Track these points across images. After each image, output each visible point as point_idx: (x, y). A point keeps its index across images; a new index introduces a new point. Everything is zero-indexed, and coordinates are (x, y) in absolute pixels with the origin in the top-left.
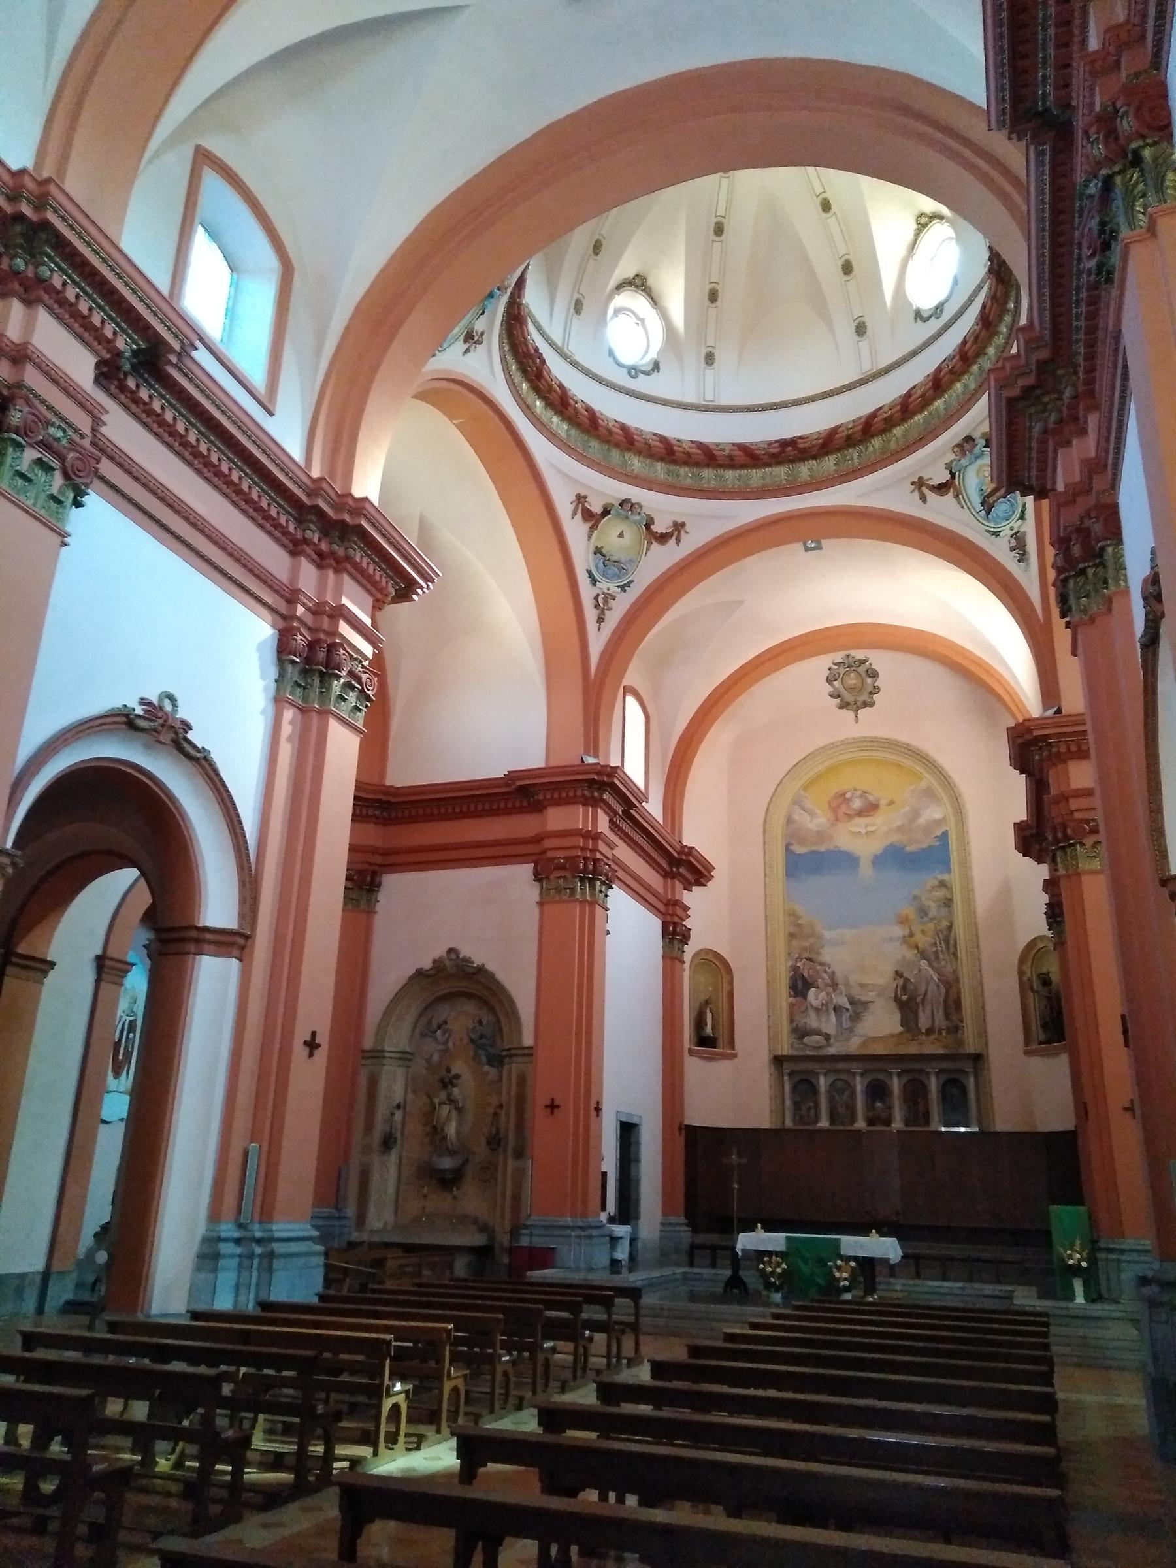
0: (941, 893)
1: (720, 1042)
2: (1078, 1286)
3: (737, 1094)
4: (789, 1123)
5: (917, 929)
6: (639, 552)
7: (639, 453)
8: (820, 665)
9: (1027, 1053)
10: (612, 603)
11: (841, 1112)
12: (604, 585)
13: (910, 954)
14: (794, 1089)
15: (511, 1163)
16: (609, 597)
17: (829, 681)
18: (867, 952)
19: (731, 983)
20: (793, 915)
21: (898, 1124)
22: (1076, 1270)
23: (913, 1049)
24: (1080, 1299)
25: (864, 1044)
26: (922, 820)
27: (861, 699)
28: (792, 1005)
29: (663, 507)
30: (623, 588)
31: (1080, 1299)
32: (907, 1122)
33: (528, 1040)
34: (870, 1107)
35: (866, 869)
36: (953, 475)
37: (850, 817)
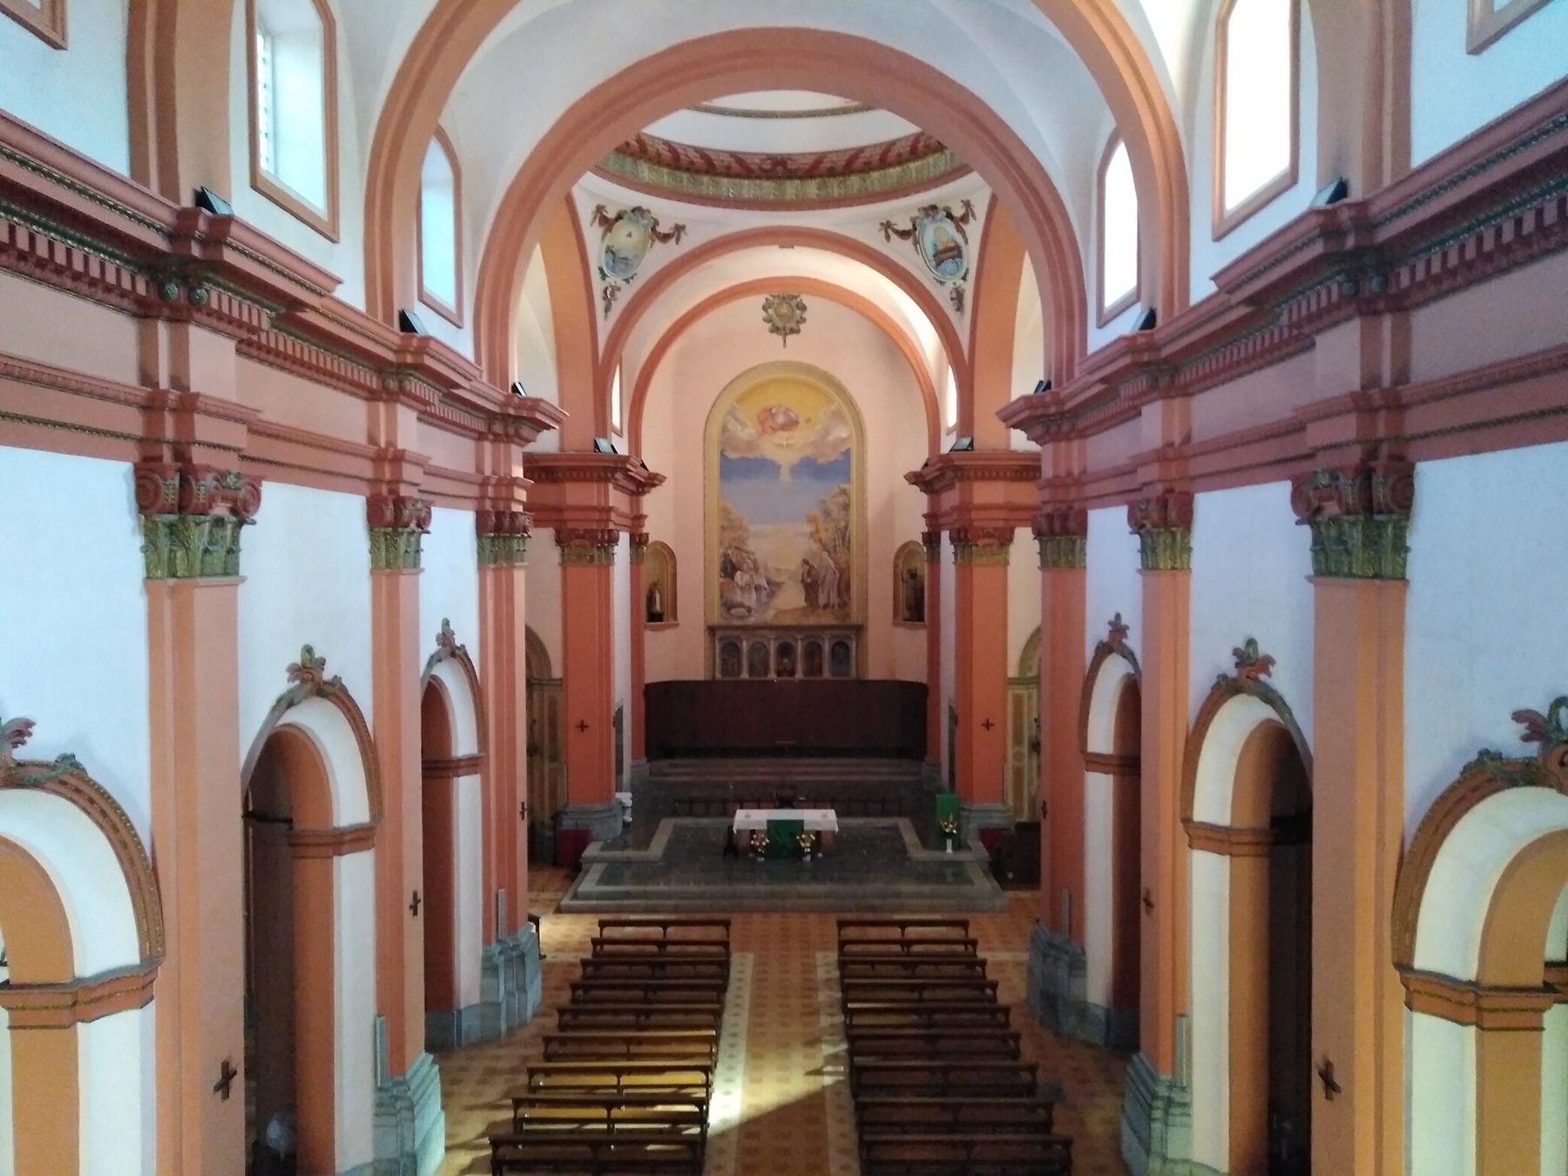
0: (841, 499)
2: (949, 843)
4: (718, 676)
5: (821, 526)
6: (644, 247)
8: (759, 300)
9: (895, 624)
10: (618, 294)
11: (759, 666)
12: (612, 279)
13: (815, 546)
14: (723, 650)
16: (616, 289)
17: (765, 308)
18: (782, 543)
19: (675, 567)
20: (725, 512)
21: (799, 676)
22: (950, 835)
23: (812, 621)
24: (949, 850)
25: (776, 616)
26: (831, 438)
27: (788, 326)
28: (722, 584)
29: (667, 211)
30: (627, 281)
31: (949, 850)
32: (805, 673)
34: (779, 663)
35: (785, 476)
37: (774, 430)
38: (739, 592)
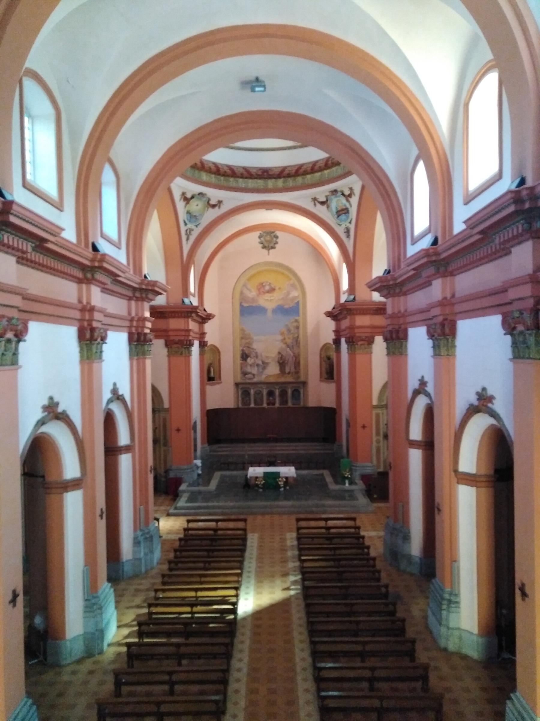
1: (216, 379)
2: (347, 481)
3: (223, 396)
4: (240, 406)
7: (206, 171)
8: (257, 233)
10: (192, 232)
12: (189, 226)
13: (284, 346)
14: (242, 394)
15: (163, 449)
16: (191, 230)
18: (269, 345)
20: (242, 330)
21: (277, 405)
22: (347, 478)
23: (282, 380)
24: (347, 485)
25: (266, 377)
28: (241, 364)
29: (214, 194)
30: (197, 226)
31: (347, 485)
33: (166, 405)
35: (269, 314)
36: (327, 200)
37: (264, 293)
38: (249, 367)
